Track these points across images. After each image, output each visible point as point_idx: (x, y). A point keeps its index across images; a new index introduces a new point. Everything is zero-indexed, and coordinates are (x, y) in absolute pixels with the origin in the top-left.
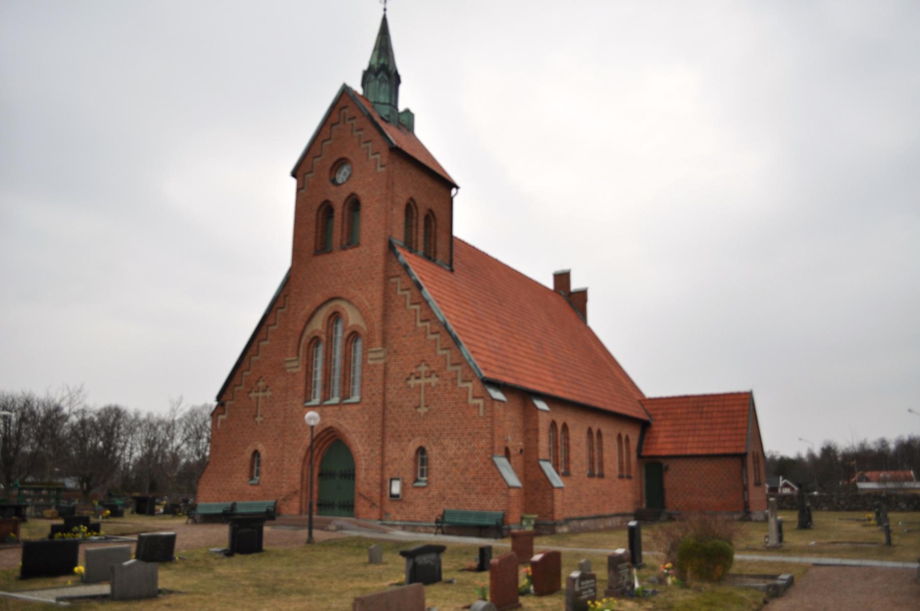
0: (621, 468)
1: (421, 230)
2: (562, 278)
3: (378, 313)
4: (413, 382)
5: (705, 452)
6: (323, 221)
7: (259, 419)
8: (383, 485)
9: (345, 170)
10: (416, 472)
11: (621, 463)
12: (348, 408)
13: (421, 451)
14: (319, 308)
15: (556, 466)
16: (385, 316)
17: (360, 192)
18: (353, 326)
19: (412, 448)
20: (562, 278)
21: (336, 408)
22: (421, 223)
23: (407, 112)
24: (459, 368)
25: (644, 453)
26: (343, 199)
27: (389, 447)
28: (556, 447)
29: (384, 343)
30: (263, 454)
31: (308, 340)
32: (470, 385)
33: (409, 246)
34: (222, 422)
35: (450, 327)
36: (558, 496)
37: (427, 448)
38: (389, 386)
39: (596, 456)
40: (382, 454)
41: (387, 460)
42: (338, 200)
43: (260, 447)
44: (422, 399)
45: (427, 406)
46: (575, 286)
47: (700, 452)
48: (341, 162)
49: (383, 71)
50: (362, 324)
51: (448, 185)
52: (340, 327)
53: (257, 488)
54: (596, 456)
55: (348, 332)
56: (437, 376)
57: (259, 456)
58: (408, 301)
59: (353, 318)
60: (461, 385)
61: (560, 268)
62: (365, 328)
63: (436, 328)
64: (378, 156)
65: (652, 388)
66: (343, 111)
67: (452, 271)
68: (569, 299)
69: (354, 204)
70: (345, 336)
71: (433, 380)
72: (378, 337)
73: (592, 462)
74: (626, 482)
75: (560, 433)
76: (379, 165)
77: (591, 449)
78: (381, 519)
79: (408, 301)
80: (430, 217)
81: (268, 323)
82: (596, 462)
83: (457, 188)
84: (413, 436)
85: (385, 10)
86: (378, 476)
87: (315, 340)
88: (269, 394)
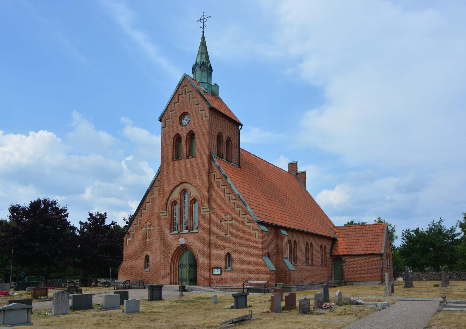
0: (322, 261)
1: (225, 148)
2: (293, 166)
3: (206, 189)
4: (223, 223)
5: (363, 253)
6: (178, 146)
7: (148, 240)
8: (211, 270)
9: (186, 117)
10: (226, 264)
11: (322, 259)
12: (192, 235)
13: (228, 254)
14: (176, 187)
15: (291, 260)
16: (210, 191)
17: (195, 130)
18: (194, 196)
19: (224, 253)
20: (293, 166)
21: (187, 235)
22: (225, 145)
23: (216, 85)
24: (246, 216)
25: (334, 254)
26: (187, 133)
27: (213, 253)
28: (291, 252)
29: (210, 204)
30: (151, 257)
31: (171, 203)
32: (251, 224)
33: (219, 155)
34: (129, 241)
35: (241, 197)
36: (292, 274)
37: (231, 253)
38: (212, 224)
39: (310, 256)
40: (210, 256)
41: (212, 259)
42: (184, 133)
43: (149, 254)
44: (228, 231)
45: (230, 234)
46: (300, 170)
47: (360, 253)
48: (184, 114)
49: (204, 66)
50: (198, 195)
51: (237, 124)
52: (186, 196)
53: (148, 273)
54: (310, 256)
55: (191, 199)
56: (235, 220)
57: (148, 257)
58: (220, 184)
59: (193, 192)
60: (247, 224)
61: (291, 161)
62: (200, 197)
63: (235, 197)
64: (203, 112)
65: (336, 225)
66: (184, 88)
67: (240, 167)
68: (297, 176)
69: (191, 135)
70: (190, 201)
71: (234, 222)
72: (206, 202)
73: (308, 259)
74: (324, 268)
75: (292, 245)
76: (204, 116)
77: (308, 252)
78: (210, 286)
79: (220, 184)
80: (229, 141)
81: (150, 194)
82: (310, 258)
83: (242, 125)
84: (224, 248)
85: (203, 32)
86: (208, 267)
87: (175, 203)
88: (152, 228)
